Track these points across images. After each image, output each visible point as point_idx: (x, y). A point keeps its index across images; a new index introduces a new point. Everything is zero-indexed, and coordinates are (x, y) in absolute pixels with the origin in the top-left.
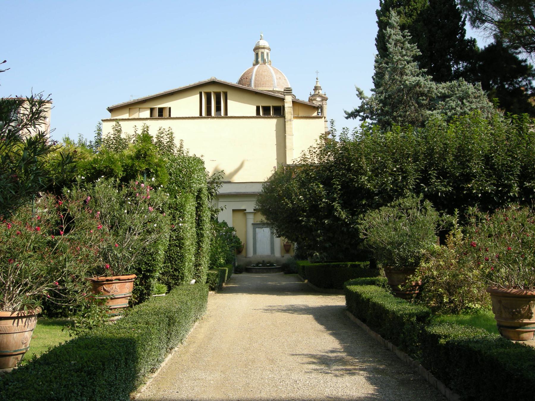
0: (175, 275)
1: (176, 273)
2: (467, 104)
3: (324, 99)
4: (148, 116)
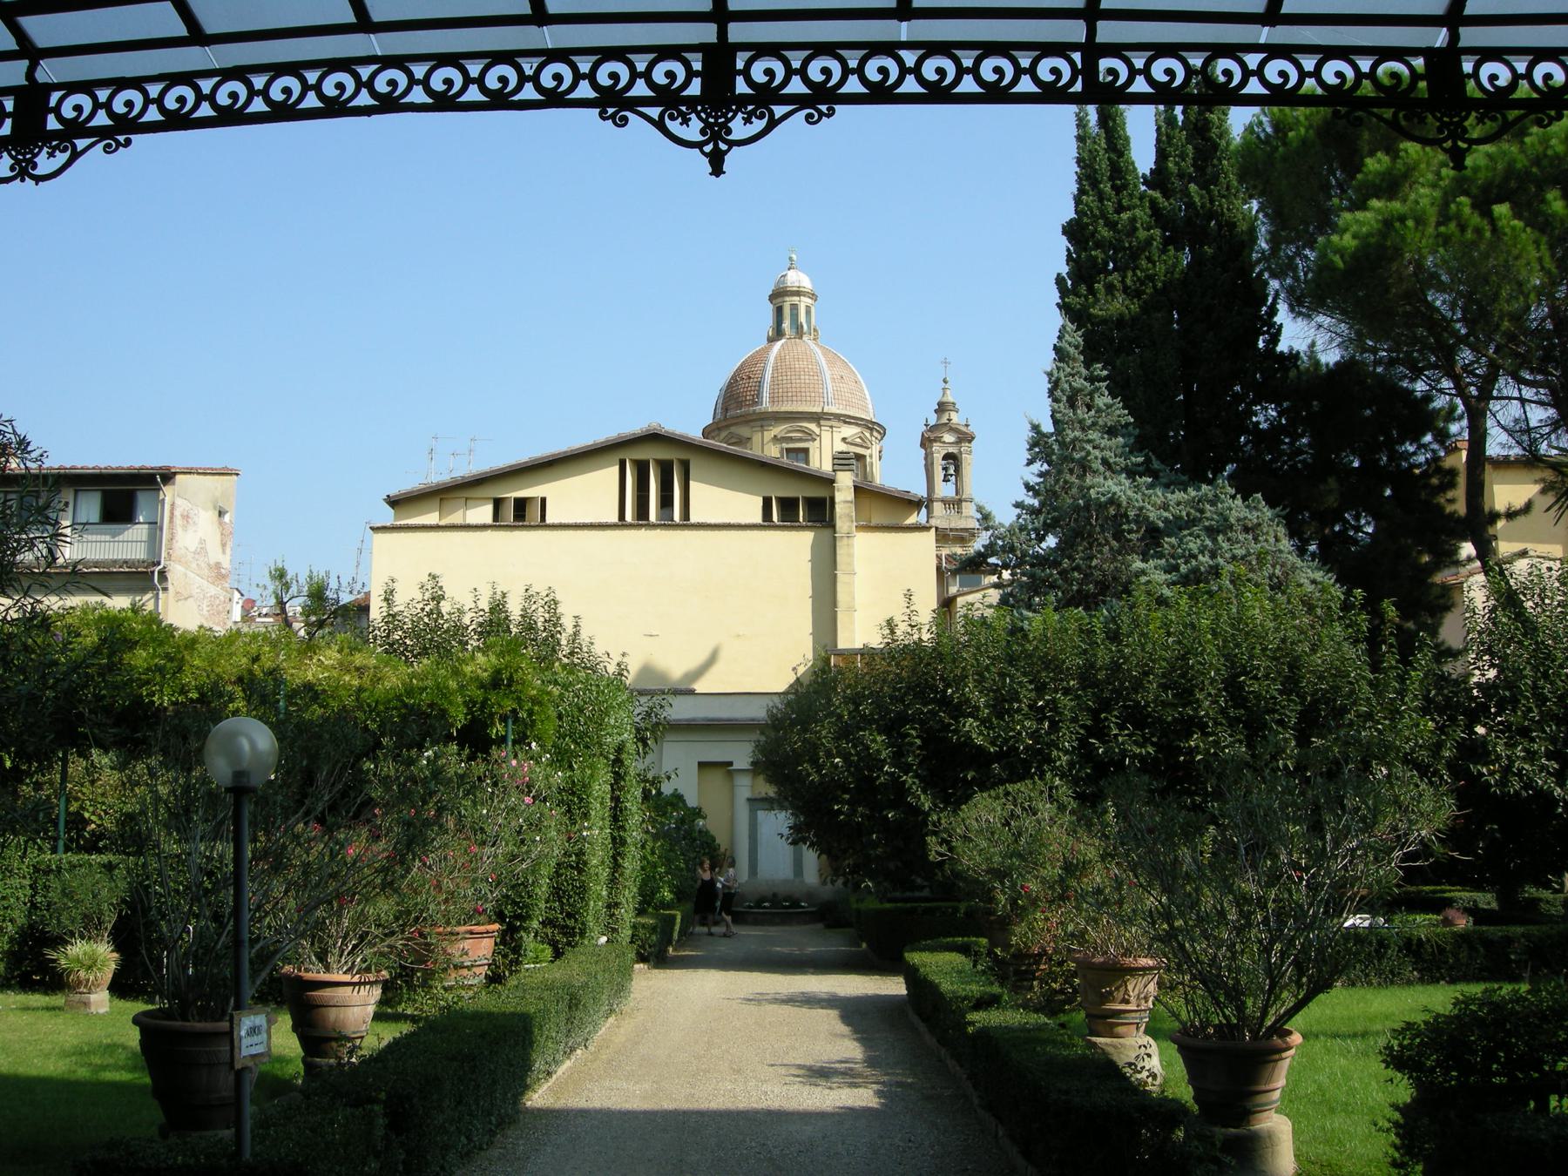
0: (567, 926)
1: (571, 923)
2: (1225, 545)
3: (965, 438)
4: (489, 519)
